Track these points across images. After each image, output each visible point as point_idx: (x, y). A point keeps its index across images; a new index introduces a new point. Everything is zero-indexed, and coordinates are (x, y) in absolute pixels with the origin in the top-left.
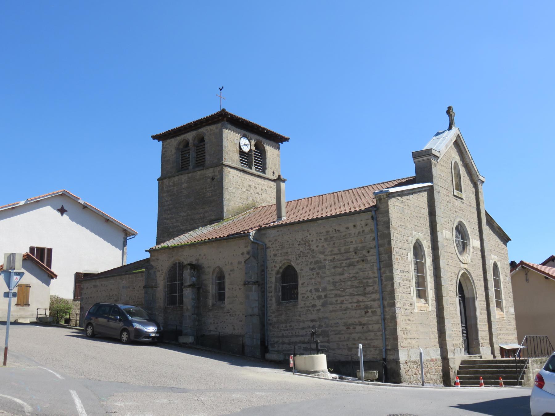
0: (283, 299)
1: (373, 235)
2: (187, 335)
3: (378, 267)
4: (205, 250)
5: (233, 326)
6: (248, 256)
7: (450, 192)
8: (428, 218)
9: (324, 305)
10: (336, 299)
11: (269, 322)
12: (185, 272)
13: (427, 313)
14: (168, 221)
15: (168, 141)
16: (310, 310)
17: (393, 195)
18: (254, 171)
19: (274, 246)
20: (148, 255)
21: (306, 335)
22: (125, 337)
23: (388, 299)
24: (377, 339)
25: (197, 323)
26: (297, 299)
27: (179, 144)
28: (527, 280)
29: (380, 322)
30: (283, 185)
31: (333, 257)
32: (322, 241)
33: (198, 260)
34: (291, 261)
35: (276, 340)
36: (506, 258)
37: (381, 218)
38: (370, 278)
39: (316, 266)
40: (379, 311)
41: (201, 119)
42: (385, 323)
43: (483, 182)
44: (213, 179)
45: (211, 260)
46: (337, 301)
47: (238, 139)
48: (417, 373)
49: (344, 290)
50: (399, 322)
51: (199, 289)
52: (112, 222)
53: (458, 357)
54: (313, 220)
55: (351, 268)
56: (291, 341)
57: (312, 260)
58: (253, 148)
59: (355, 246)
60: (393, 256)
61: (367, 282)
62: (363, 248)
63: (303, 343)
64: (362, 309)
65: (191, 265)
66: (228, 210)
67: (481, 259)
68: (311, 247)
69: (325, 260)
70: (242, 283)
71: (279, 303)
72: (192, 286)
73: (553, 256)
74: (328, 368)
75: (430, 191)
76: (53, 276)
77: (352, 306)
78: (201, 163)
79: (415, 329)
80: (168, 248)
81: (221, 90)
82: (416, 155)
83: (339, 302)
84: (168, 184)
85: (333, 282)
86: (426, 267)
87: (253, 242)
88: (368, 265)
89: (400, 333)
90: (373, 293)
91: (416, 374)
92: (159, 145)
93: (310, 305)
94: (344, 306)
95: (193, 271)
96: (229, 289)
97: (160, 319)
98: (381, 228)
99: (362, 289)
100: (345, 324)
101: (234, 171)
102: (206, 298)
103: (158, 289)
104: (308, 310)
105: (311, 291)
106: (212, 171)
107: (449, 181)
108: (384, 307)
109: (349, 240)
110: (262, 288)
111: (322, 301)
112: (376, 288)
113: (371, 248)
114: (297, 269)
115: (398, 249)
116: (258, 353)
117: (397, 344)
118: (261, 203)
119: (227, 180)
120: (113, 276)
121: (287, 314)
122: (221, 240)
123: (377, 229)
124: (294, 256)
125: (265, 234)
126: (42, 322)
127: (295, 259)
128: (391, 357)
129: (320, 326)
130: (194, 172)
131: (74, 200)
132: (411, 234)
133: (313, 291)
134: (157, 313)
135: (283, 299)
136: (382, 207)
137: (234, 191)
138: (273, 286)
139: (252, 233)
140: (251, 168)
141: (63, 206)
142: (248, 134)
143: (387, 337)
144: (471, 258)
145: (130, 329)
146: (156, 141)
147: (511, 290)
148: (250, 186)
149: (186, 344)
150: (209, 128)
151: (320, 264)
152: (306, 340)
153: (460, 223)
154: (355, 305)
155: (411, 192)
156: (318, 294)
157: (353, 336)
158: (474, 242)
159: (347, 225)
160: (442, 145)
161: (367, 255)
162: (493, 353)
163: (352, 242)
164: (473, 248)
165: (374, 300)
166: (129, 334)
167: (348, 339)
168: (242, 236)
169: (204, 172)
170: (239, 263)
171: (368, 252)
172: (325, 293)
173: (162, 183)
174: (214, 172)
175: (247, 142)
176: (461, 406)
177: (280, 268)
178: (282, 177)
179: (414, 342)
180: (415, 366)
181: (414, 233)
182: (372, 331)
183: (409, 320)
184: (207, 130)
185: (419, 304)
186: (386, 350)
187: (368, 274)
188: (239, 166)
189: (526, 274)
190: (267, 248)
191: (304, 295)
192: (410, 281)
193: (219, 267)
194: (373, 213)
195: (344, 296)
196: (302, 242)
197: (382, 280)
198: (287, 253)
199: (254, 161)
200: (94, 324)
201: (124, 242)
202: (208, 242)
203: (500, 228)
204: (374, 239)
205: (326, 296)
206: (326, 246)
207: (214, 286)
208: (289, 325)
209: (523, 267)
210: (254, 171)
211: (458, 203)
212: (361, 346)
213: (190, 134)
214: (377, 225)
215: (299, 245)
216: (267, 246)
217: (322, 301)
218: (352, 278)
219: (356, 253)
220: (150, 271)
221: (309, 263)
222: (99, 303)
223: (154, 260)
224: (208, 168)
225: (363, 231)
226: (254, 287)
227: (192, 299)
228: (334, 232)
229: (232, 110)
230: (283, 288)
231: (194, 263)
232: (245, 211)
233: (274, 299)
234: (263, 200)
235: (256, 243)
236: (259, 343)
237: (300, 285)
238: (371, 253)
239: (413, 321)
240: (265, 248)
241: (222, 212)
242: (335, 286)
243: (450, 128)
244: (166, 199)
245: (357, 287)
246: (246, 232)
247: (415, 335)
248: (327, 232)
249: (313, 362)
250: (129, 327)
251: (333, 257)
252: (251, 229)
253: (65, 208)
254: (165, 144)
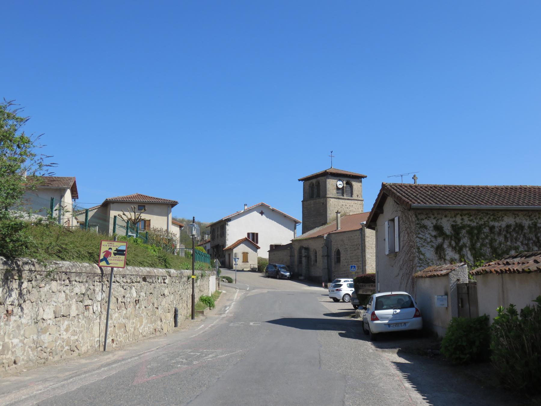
18: (345, 197)
27: (310, 184)
45: (313, 246)
58: (345, 185)
71: (335, 264)
72: (305, 256)
76: (258, 248)
78: (318, 196)
92: (302, 183)
101: (333, 199)
126: (253, 270)
131: (267, 207)
139: (325, 236)
175: (341, 183)
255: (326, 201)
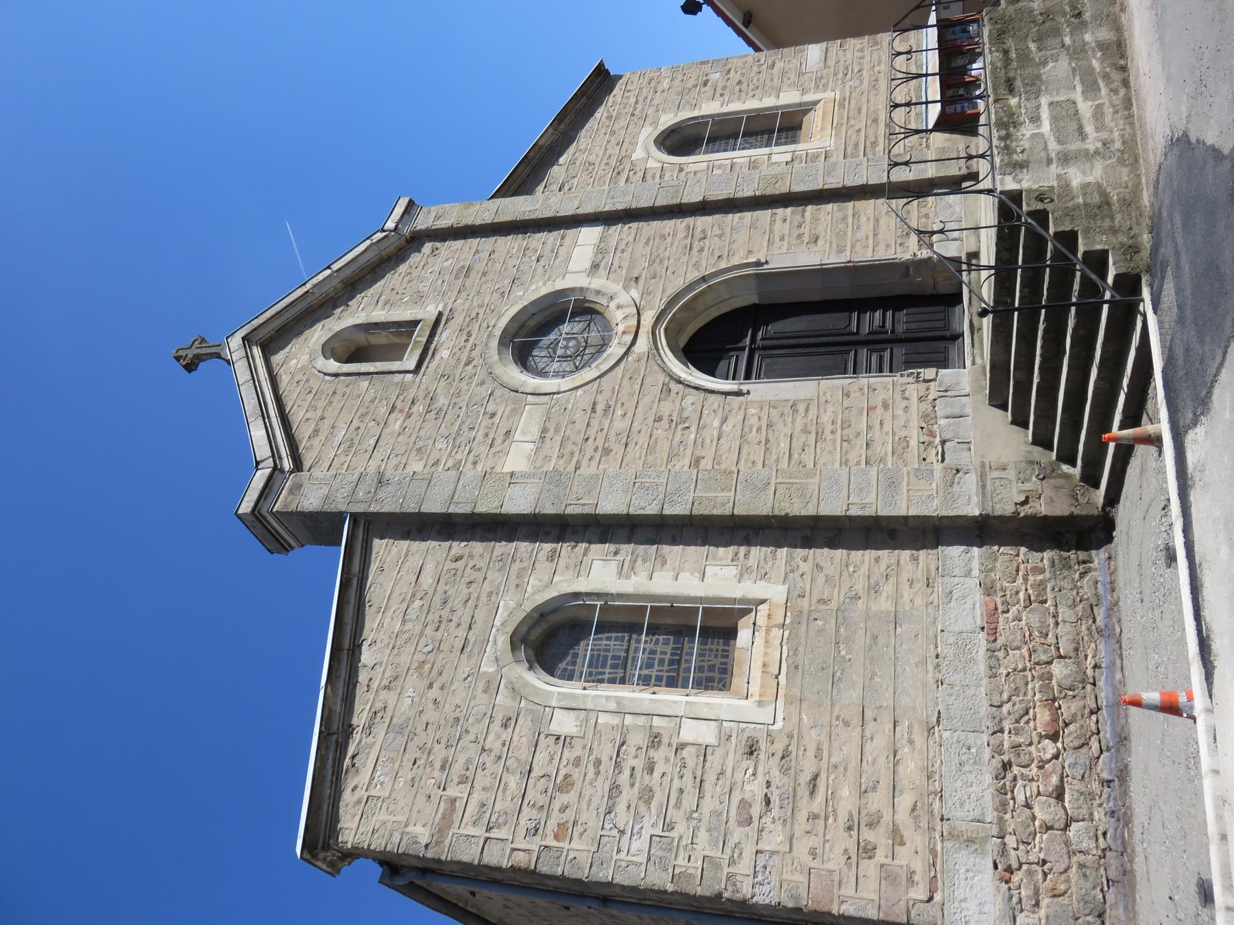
7: (403, 387)
86: (620, 596)
176: (1211, 696)
203: (560, 118)
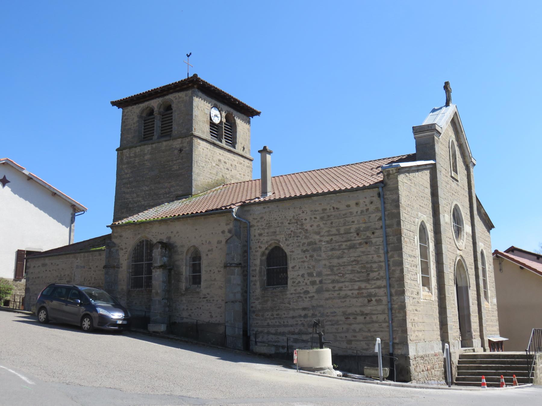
0: (269, 284)
1: (379, 214)
2: (156, 322)
3: (385, 250)
4: (178, 227)
5: (210, 313)
6: (229, 235)
7: (448, 172)
8: (430, 198)
9: (319, 291)
10: (334, 285)
11: (252, 309)
12: (154, 251)
13: (431, 302)
14: (127, 196)
15: (130, 108)
16: (301, 297)
17: (403, 170)
19: (259, 224)
20: (109, 231)
21: (297, 324)
22: (86, 324)
23: (396, 286)
24: (382, 331)
25: (167, 309)
26: (287, 284)
27: (143, 111)
28: (500, 270)
29: (386, 311)
30: (268, 157)
31: (331, 237)
32: (317, 220)
33: (169, 238)
34: (279, 241)
35: (260, 329)
36: (490, 246)
37: (389, 196)
38: (375, 262)
39: (309, 248)
40: (385, 299)
41: (170, 85)
42: (392, 313)
43: (474, 165)
44: (181, 150)
45: (186, 238)
46: (334, 287)
47: (209, 108)
48: (424, 370)
49: (343, 275)
50: (408, 313)
51: (170, 270)
52: (59, 196)
53: (457, 350)
54: (307, 196)
55: (351, 250)
56: (279, 331)
57: (306, 241)
58: (224, 120)
59: (357, 226)
60: (402, 238)
61: (371, 267)
62: (367, 229)
63: (293, 333)
64: (365, 297)
65: (161, 242)
66: (197, 186)
67: (472, 245)
68: (304, 226)
69: (320, 241)
70: (222, 265)
71: (264, 289)
73: (513, 247)
74: (333, 364)
75: (433, 169)
77: (352, 294)
78: (167, 132)
79: (421, 321)
80: (134, 224)
81: (188, 56)
82: (417, 130)
83: (336, 288)
84: (128, 155)
85: (330, 266)
87: (235, 219)
88: (373, 248)
89: (409, 325)
90: (378, 279)
91: (423, 371)
92: (118, 112)
93: (302, 291)
94: (343, 293)
95: (164, 250)
96: (206, 271)
97: (123, 303)
98: (388, 206)
99: (365, 274)
100: (344, 313)
102: (179, 281)
103: (121, 269)
104: (298, 297)
105: (303, 276)
106: (180, 142)
107: (446, 160)
108: (391, 295)
109: (350, 219)
110: (243, 271)
111: (316, 287)
112: (382, 273)
113: (377, 229)
114: (287, 250)
115: (406, 231)
116: (240, 344)
117: (407, 337)
118: (231, 180)
119: (197, 153)
120: (65, 254)
121: (273, 301)
122: (198, 216)
123: (384, 207)
124: (283, 236)
125: (248, 211)
127: (284, 239)
128: (399, 352)
129: (314, 315)
130: (159, 142)
131: (18, 170)
132: (417, 215)
133: (306, 276)
134: (119, 296)
135: (269, 284)
136: (390, 183)
137: (203, 165)
138: (258, 269)
139: (235, 209)
140: (221, 142)
141: (5, 177)
142: (219, 104)
143: (395, 329)
144: (465, 242)
145: (93, 314)
146: (116, 107)
147: (494, 279)
148: (220, 160)
149: (157, 332)
150: (177, 95)
151: (315, 246)
152: (297, 331)
153: (456, 205)
154: (356, 292)
155: (420, 168)
156: (311, 279)
157: (353, 327)
158: (467, 228)
159: (348, 203)
160: (442, 120)
161: (372, 236)
162: (483, 345)
163: (353, 222)
164: (467, 233)
165: (379, 287)
166: (91, 320)
167: (348, 330)
168: (222, 212)
169: (170, 143)
170: (219, 242)
171: (373, 233)
172: (320, 279)
173: (122, 154)
174: (182, 143)
175: (217, 113)
177: (266, 249)
178: (268, 148)
179: (420, 334)
180: (422, 361)
181: (420, 214)
182: (376, 322)
183: (416, 310)
184: (174, 97)
185: (424, 292)
186: (394, 344)
187: (373, 257)
188: (209, 137)
189: (500, 264)
190: (251, 227)
191: (294, 280)
192: (416, 267)
193: (194, 246)
194: (380, 190)
195: (343, 282)
196: (293, 221)
197: (389, 265)
198: (275, 232)
199: (224, 134)
200: (48, 308)
201: (72, 218)
202: (183, 218)
204: (380, 219)
205: (321, 282)
206: (322, 226)
207: (188, 268)
208: (277, 313)
209: (497, 256)
210: (224, 144)
211: (454, 184)
212: (379, 340)
213: (155, 100)
214: (384, 203)
215: (289, 223)
216: (251, 224)
217: (316, 287)
218: (353, 261)
219: (358, 234)
220: (112, 249)
221: (301, 244)
222: (54, 284)
223: (116, 237)
224: (175, 139)
225: (367, 210)
226: (237, 270)
227: (163, 282)
228: (332, 210)
229: (204, 77)
230: (269, 272)
231: (165, 241)
232: (215, 187)
233: (258, 284)
234: (232, 176)
235: (239, 220)
236: (241, 333)
237: (290, 269)
238: (376, 234)
239: (419, 311)
240: (248, 227)
241: (191, 187)
242: (332, 270)
243: (447, 105)
244: (126, 171)
245: (358, 272)
246: (228, 207)
247: (421, 327)
248: (324, 210)
249: (318, 357)
250: (91, 312)
251: (331, 237)
252: (234, 205)
253: (8, 178)
254: (126, 111)
255: (191, 145)
